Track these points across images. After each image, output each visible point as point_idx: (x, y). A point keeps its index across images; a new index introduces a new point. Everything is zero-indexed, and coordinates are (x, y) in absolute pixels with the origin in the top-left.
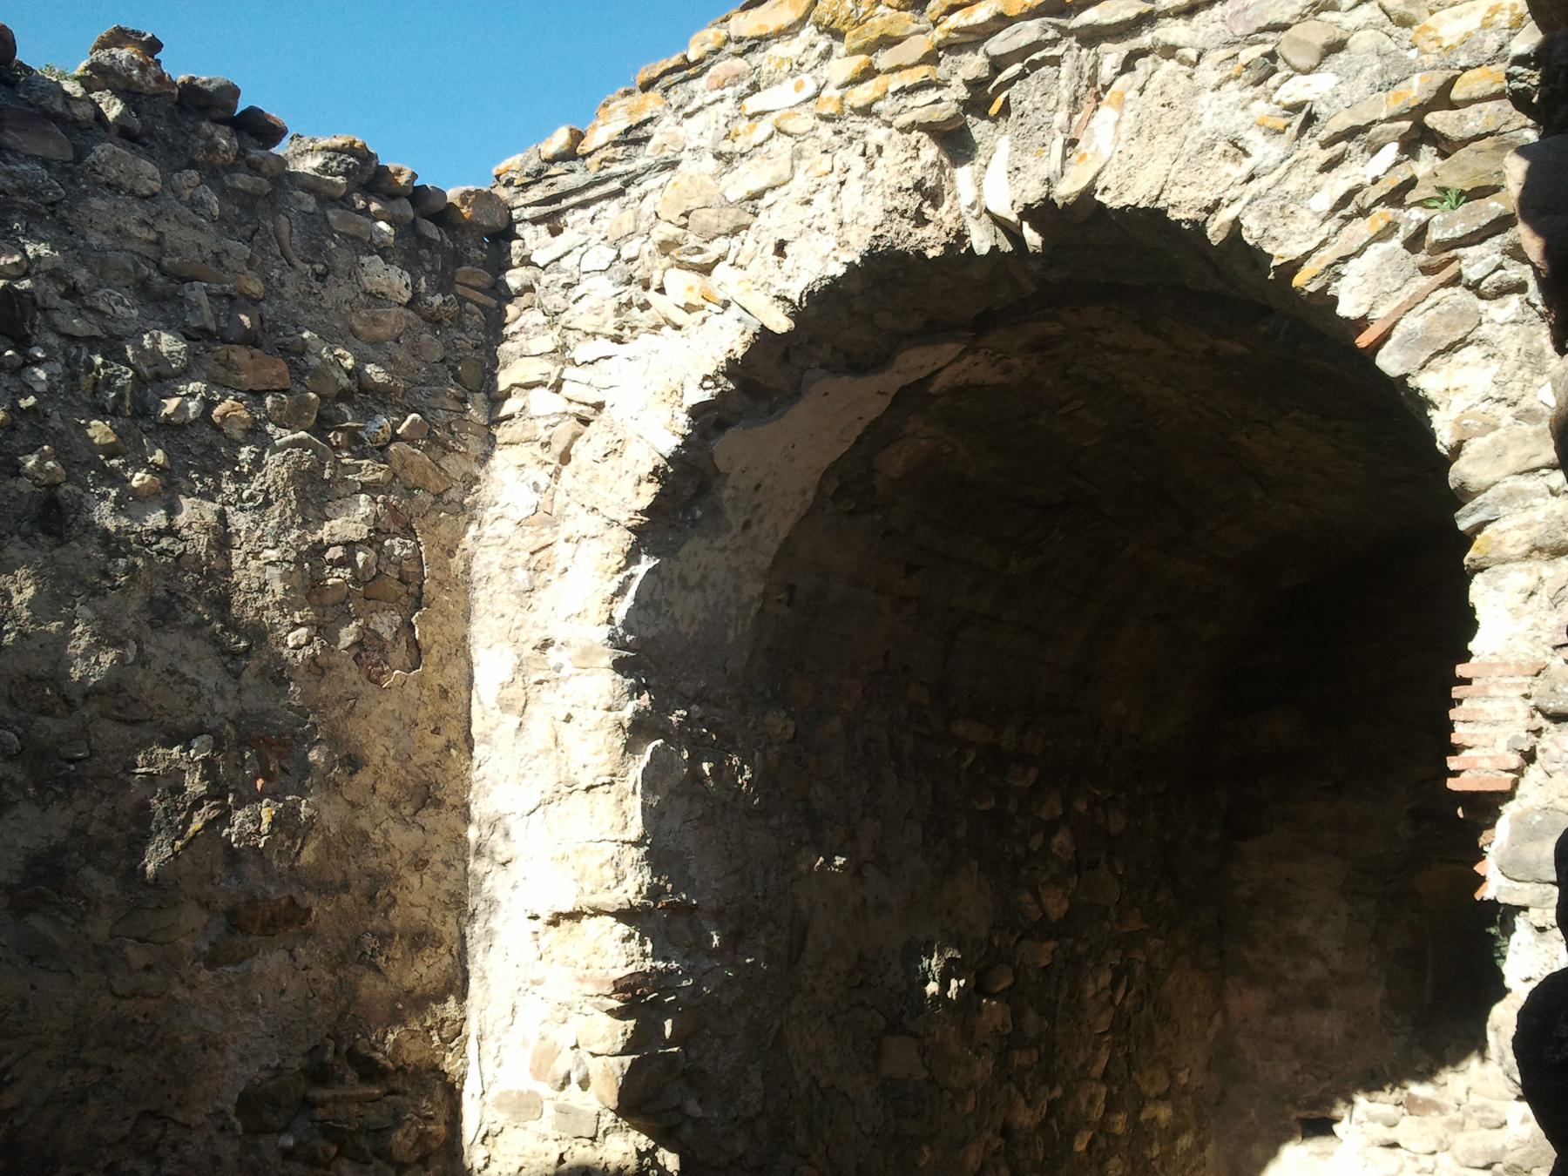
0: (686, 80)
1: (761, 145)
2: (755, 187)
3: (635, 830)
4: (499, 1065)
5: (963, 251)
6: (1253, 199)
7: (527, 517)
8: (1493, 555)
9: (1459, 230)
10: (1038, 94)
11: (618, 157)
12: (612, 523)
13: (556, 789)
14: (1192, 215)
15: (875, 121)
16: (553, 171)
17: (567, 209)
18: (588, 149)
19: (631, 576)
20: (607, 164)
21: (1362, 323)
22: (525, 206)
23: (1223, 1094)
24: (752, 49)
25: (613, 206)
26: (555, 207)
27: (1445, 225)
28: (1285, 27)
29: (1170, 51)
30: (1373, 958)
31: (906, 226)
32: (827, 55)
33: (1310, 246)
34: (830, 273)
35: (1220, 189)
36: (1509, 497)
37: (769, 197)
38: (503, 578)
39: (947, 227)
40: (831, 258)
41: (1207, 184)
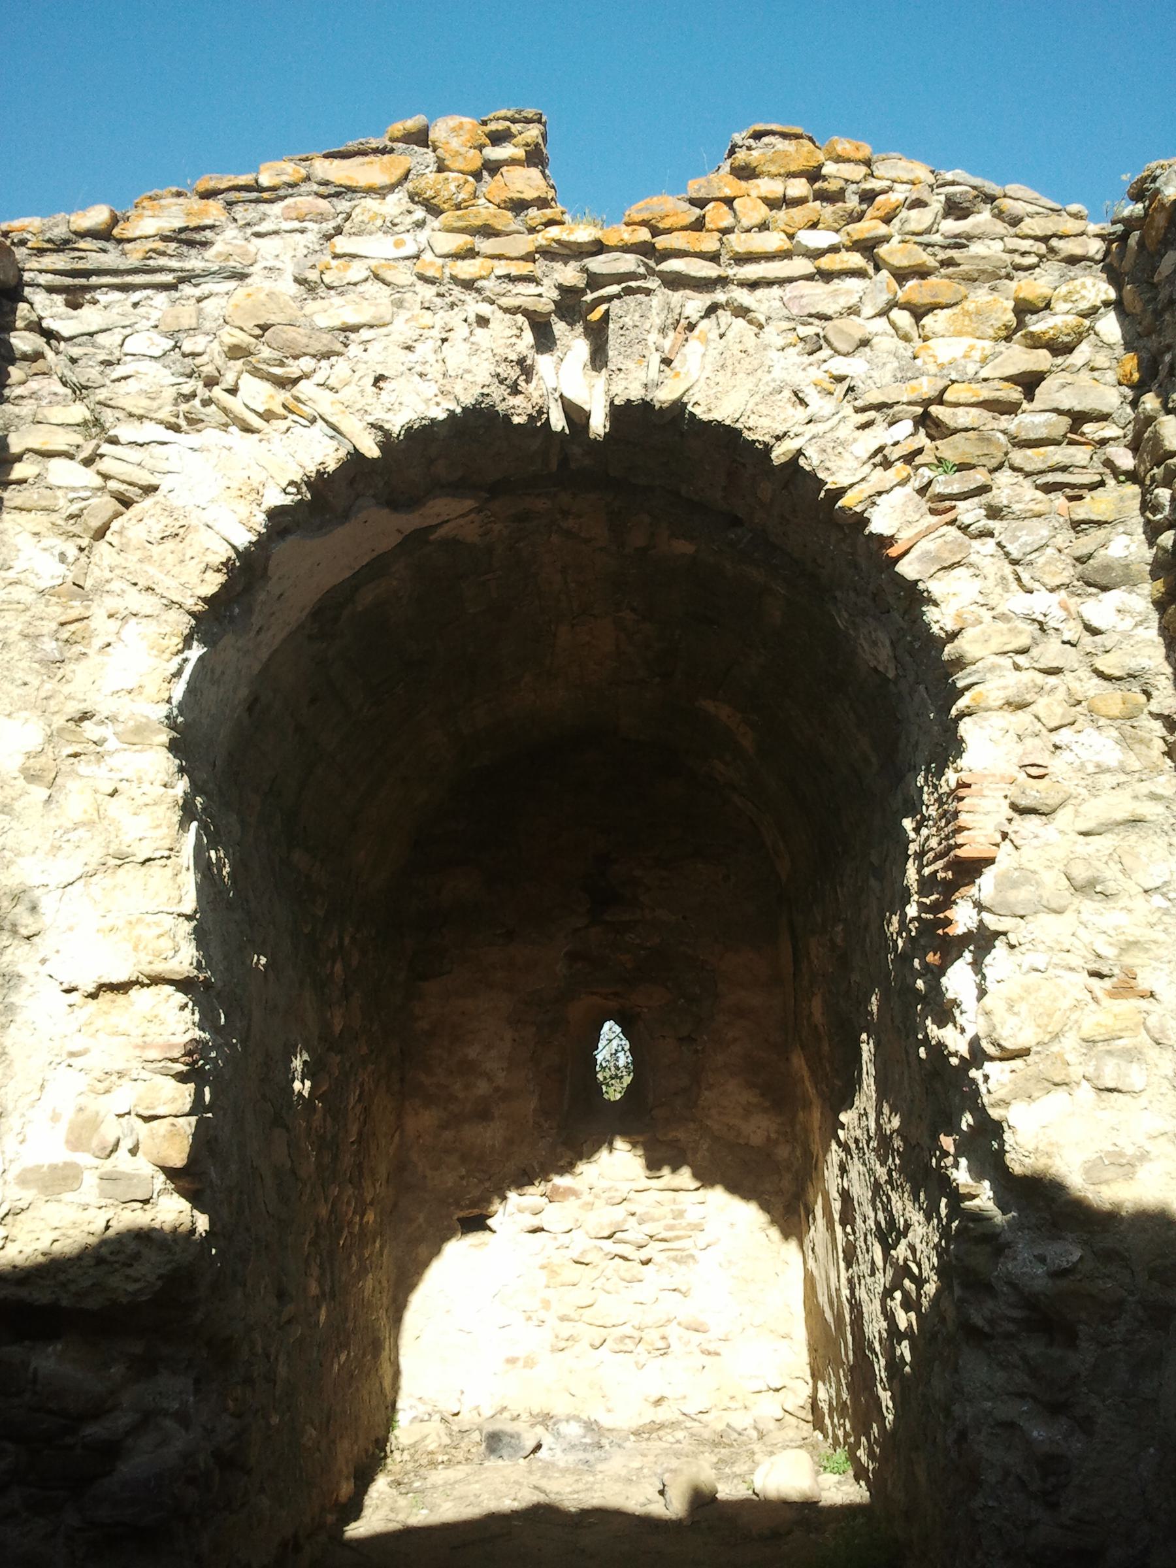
0: (257, 201)
1: (355, 284)
2: (352, 320)
3: (189, 904)
4: (22, 1142)
5: (539, 424)
6: (813, 437)
7: (53, 587)
8: (982, 705)
9: (955, 489)
10: (637, 315)
11: (169, 252)
12: (171, 604)
13: (103, 861)
14: (767, 439)
15: (474, 295)
16: (82, 244)
17: (100, 287)
18: (129, 234)
19: (185, 660)
20: (154, 255)
21: (890, 541)
22: (40, 271)
23: (395, 1205)
24: (337, 195)
25: (161, 298)
26: (82, 281)
27: (946, 483)
28: (828, 318)
29: (742, 312)
30: (531, 1076)
31: (503, 391)
32: (420, 224)
33: (855, 480)
34: (433, 416)
35: (788, 425)
36: (992, 669)
37: (365, 334)
38: (24, 645)
39: (534, 401)
40: (433, 402)
41: (778, 418)
